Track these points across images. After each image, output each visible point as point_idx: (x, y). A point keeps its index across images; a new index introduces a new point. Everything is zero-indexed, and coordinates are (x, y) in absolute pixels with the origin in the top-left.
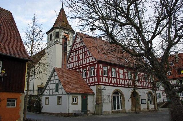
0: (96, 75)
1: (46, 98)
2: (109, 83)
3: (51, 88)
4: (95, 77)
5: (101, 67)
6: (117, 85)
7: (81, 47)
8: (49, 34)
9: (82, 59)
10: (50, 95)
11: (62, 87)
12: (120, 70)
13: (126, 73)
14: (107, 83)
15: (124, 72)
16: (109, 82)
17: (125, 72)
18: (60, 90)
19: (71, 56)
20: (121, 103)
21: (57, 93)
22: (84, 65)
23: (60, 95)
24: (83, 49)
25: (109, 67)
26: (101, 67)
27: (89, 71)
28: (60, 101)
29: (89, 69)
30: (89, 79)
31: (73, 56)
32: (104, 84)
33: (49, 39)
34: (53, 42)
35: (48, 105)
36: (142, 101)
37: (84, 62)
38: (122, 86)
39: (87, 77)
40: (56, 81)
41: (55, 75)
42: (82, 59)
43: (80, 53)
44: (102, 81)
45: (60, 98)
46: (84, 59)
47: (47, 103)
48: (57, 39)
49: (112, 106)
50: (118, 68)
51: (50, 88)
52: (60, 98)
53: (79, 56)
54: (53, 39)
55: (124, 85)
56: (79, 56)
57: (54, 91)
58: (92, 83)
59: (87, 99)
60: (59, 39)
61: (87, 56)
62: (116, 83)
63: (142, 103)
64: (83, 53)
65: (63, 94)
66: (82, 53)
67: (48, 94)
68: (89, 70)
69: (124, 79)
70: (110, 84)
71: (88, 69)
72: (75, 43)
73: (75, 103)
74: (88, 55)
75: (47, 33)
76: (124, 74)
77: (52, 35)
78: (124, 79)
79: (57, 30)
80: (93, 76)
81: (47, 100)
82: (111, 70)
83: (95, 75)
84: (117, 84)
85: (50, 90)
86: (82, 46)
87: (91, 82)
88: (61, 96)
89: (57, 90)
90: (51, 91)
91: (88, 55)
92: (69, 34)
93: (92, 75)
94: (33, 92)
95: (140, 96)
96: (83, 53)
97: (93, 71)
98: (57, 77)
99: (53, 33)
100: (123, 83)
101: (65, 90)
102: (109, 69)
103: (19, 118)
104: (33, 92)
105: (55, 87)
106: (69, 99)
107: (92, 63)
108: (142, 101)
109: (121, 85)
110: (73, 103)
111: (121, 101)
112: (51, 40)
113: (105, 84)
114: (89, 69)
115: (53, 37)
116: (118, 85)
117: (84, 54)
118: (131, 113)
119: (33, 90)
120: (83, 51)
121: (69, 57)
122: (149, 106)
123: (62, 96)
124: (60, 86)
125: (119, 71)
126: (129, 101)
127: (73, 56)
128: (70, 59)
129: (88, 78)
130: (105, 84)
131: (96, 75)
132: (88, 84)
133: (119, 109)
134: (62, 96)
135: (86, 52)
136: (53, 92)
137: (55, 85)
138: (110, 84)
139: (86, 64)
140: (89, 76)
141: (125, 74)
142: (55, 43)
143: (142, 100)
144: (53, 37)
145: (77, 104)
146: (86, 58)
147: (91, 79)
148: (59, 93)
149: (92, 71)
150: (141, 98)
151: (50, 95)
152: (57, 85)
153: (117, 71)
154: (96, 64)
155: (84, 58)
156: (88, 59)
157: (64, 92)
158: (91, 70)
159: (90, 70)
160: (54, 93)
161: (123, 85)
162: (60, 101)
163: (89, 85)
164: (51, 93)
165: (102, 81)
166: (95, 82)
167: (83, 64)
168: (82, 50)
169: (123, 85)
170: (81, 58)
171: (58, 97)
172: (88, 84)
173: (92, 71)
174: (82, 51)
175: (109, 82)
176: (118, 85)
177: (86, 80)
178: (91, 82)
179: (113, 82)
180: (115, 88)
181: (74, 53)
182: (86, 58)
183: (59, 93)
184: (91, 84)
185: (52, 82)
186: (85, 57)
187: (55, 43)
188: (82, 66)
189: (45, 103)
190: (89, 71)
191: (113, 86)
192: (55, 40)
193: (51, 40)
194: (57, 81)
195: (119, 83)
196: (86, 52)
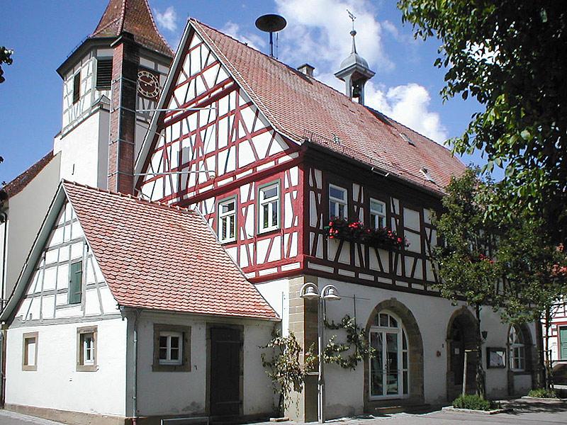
0: (288, 224)
1: (29, 340)
2: (357, 270)
3: (49, 286)
4: (287, 236)
5: (319, 186)
6: (394, 280)
7: (209, 92)
9: (215, 153)
10: (42, 322)
11: (101, 278)
12: (406, 211)
13: (432, 227)
14: (344, 267)
15: (423, 225)
16: (357, 264)
17: (428, 226)
18: (90, 296)
19: (161, 143)
20: (405, 366)
21: (75, 311)
22: (223, 178)
23: (89, 318)
24: (223, 102)
25: (356, 189)
26: (319, 186)
27: (251, 208)
28: (89, 351)
29: (252, 197)
30: (251, 246)
31: (168, 140)
32: (331, 270)
35: (34, 368)
36: (491, 364)
37: (225, 163)
38: (414, 286)
39: (238, 235)
41: (68, 218)
42: (215, 153)
43: (203, 123)
44: (320, 255)
45: (87, 337)
46: (228, 148)
47: (31, 363)
48: (104, 92)
49: (366, 381)
50: (396, 202)
51: (45, 289)
52: (87, 337)
53: (198, 139)
54: (86, 94)
55: (424, 281)
56: (198, 139)
57: (63, 299)
58: (267, 265)
59: (242, 344)
61: (242, 134)
62: (386, 270)
63: (488, 367)
64: (218, 118)
65: (102, 317)
66: (216, 122)
67: (36, 316)
68: (249, 202)
69: (422, 255)
70: (361, 276)
71: (244, 199)
72: (182, 78)
73: (174, 362)
74: (244, 126)
76: (422, 234)
77: (83, 77)
78: (422, 255)
79: (103, 53)
80: (271, 228)
81: (31, 346)
82: (367, 207)
83: (283, 223)
84: (392, 275)
85: (45, 299)
86: (217, 86)
87: (260, 260)
88: (92, 324)
89: (76, 297)
90: (49, 302)
91: (244, 126)
92: (158, 74)
93: (266, 226)
95: (485, 334)
96: (218, 118)
97: (275, 204)
98: (78, 230)
100: (419, 275)
101: (115, 292)
102: (355, 198)
105: (64, 283)
106: (41, 305)
107: (272, 164)
108: (492, 355)
109: (412, 280)
110: (163, 362)
111: (405, 354)
113: (336, 271)
114: (252, 197)
116: (398, 283)
117: (223, 124)
120: (223, 111)
121: (152, 150)
122: (515, 377)
123: (101, 325)
124: (93, 272)
125: (401, 217)
126: (439, 354)
127: (168, 140)
128: (156, 158)
129: (246, 242)
130: (336, 271)
131: (288, 224)
132: (247, 270)
133: (165, 358)
134: (101, 325)
135: (235, 113)
136: (57, 308)
137: (65, 271)
138: (361, 276)
139: (233, 174)
140: (250, 230)
141: (428, 230)
142: (93, 107)
143: (488, 350)
145: (185, 366)
146: (233, 143)
147: (263, 245)
148: (83, 309)
149: (266, 207)
150: (487, 342)
151: (42, 322)
152: (77, 270)
153: (394, 215)
154: (287, 166)
155: (223, 142)
156: (245, 146)
157: (111, 306)
158: (262, 201)
159: (255, 202)
160: (61, 314)
161: (418, 281)
162: (89, 351)
163: (252, 275)
164: (48, 314)
165: (320, 255)
166: (286, 260)
167: (221, 172)
168: (217, 106)
169: (418, 281)
170: (210, 147)
172: (247, 270)
173: (266, 207)
174: (217, 111)
175: (357, 264)
176: (398, 283)
177: (232, 252)
178: (260, 260)
179: (374, 265)
180: (381, 295)
181: (176, 126)
182: (233, 143)
183: (83, 309)
184: (263, 273)
185: (51, 257)
186: (230, 138)
187: (93, 107)
188: (223, 87)
189: (20, 360)
190: (251, 208)
191: (375, 284)
192: (93, 95)
194: (78, 251)
195: (399, 273)
196: (235, 113)
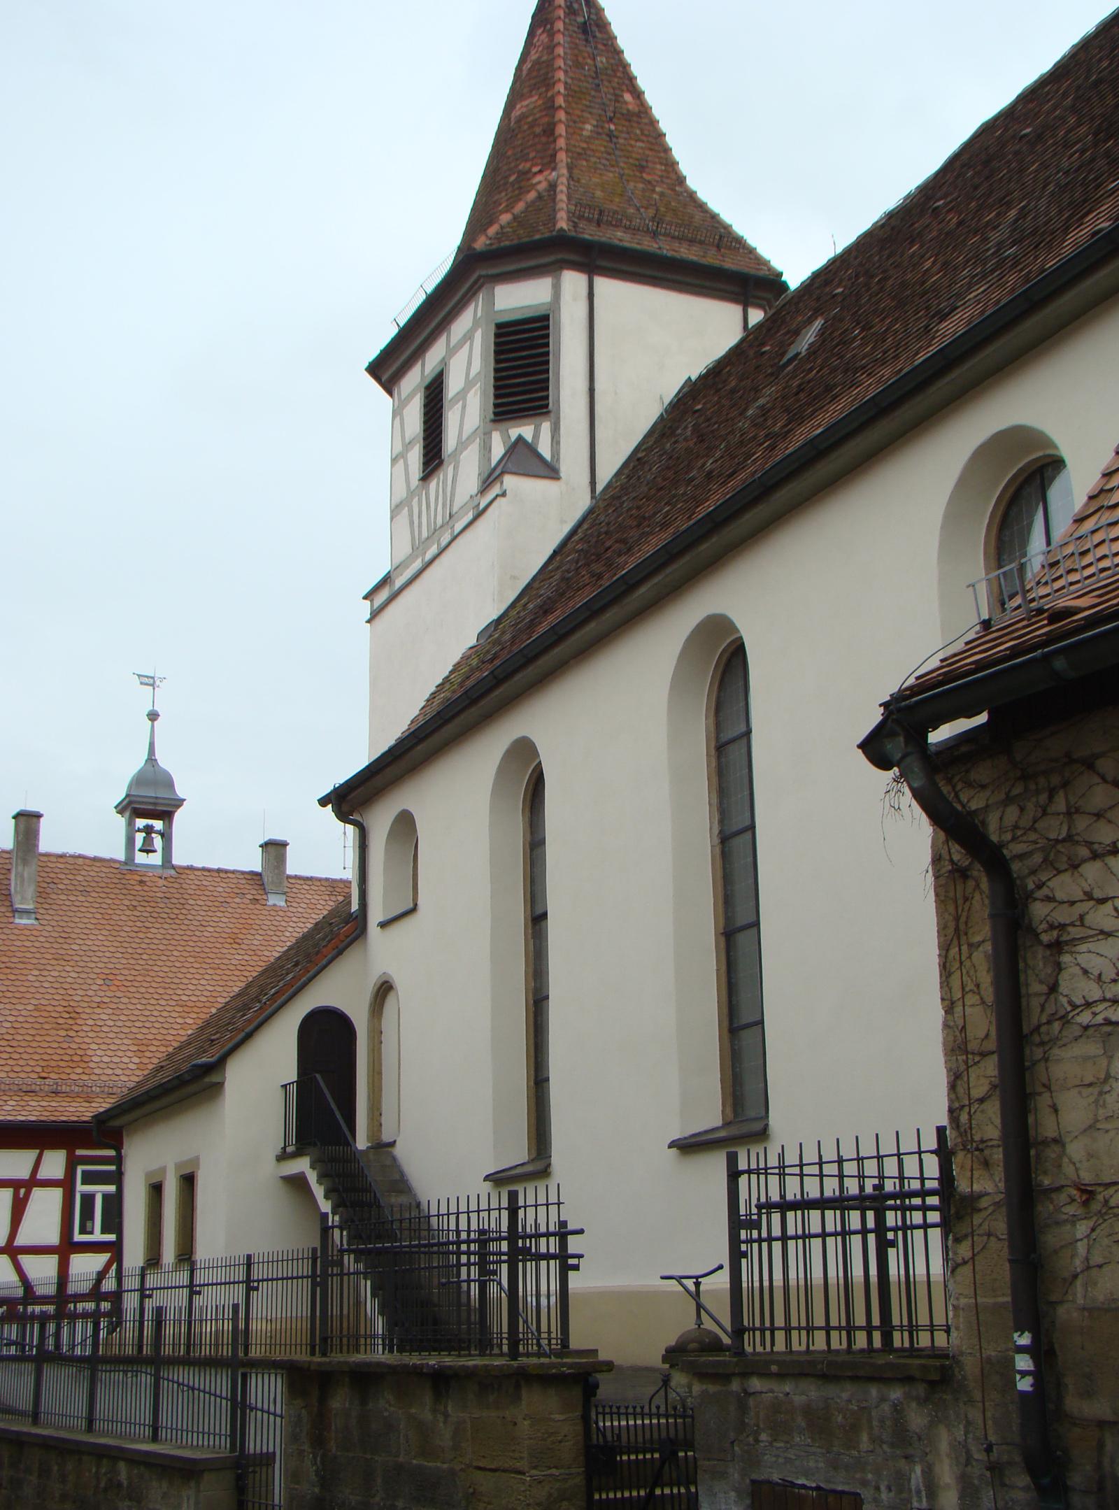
8: (414, 380)
33: (415, 456)
34: (464, 472)
40: (218, 1419)
48: (525, 431)
60: (546, 427)
75: (387, 369)
77: (453, 386)
94: (921, 1161)
99: (465, 358)
103: (497, 642)
104: (921, 1161)
112: (433, 456)
115: (467, 412)
118: (960, 946)
119: (920, 1153)
144: (467, 412)
171: (347, 883)
192: (486, 448)
193: (433, 456)
